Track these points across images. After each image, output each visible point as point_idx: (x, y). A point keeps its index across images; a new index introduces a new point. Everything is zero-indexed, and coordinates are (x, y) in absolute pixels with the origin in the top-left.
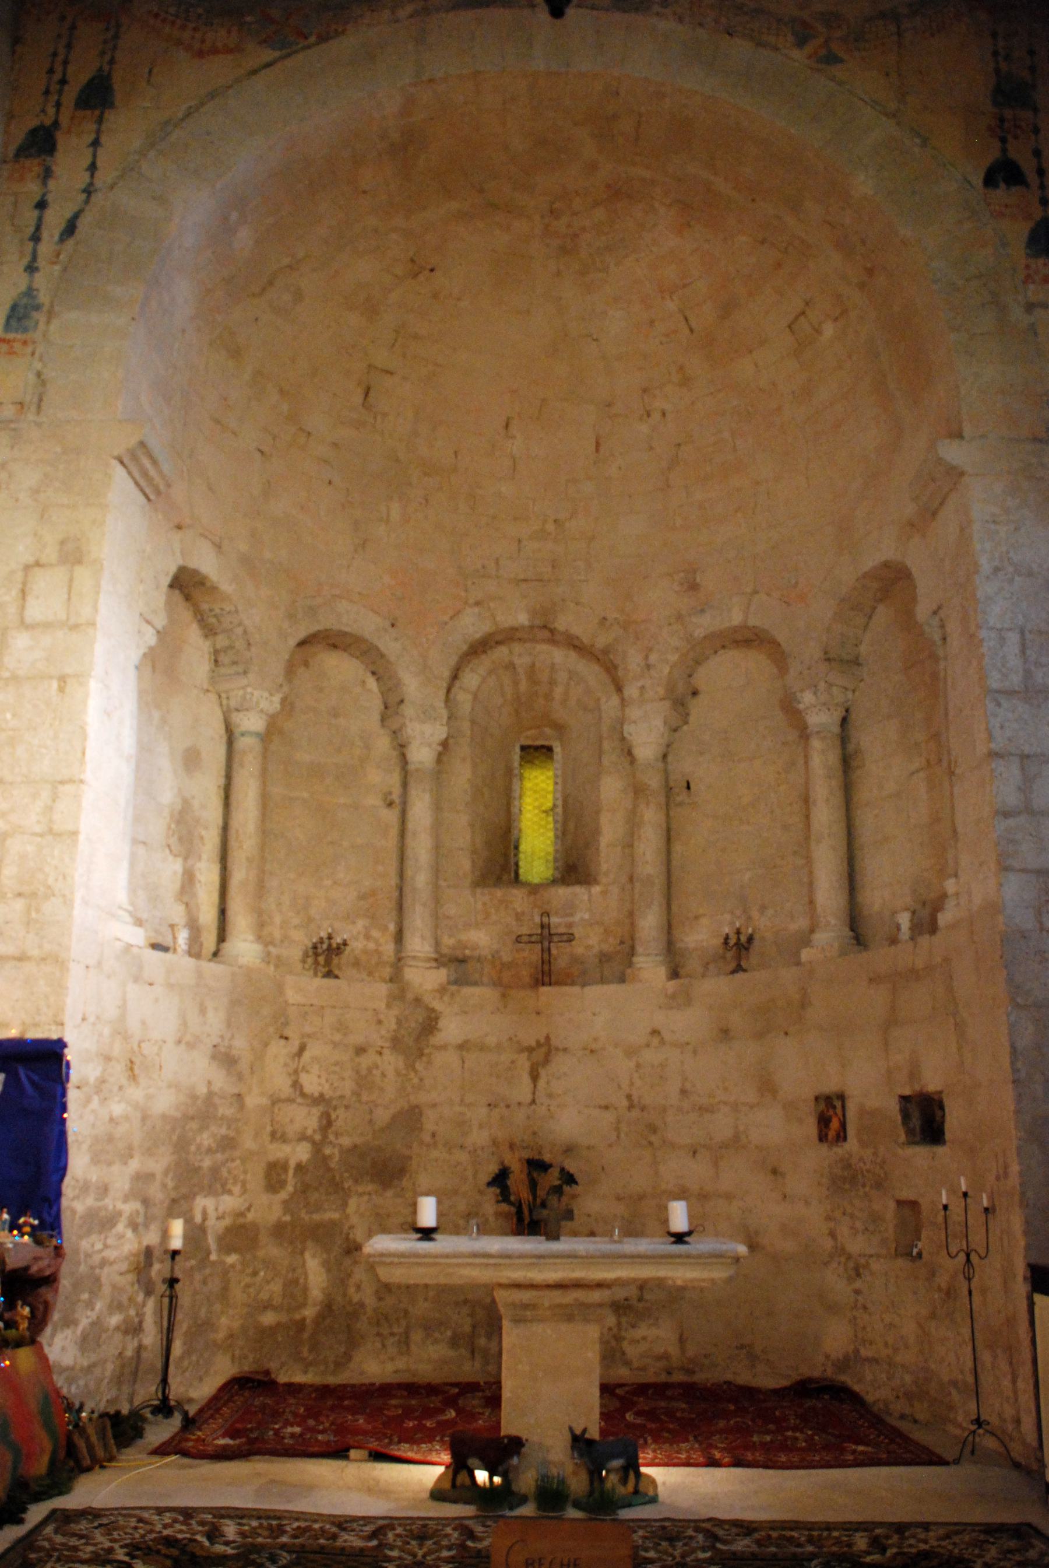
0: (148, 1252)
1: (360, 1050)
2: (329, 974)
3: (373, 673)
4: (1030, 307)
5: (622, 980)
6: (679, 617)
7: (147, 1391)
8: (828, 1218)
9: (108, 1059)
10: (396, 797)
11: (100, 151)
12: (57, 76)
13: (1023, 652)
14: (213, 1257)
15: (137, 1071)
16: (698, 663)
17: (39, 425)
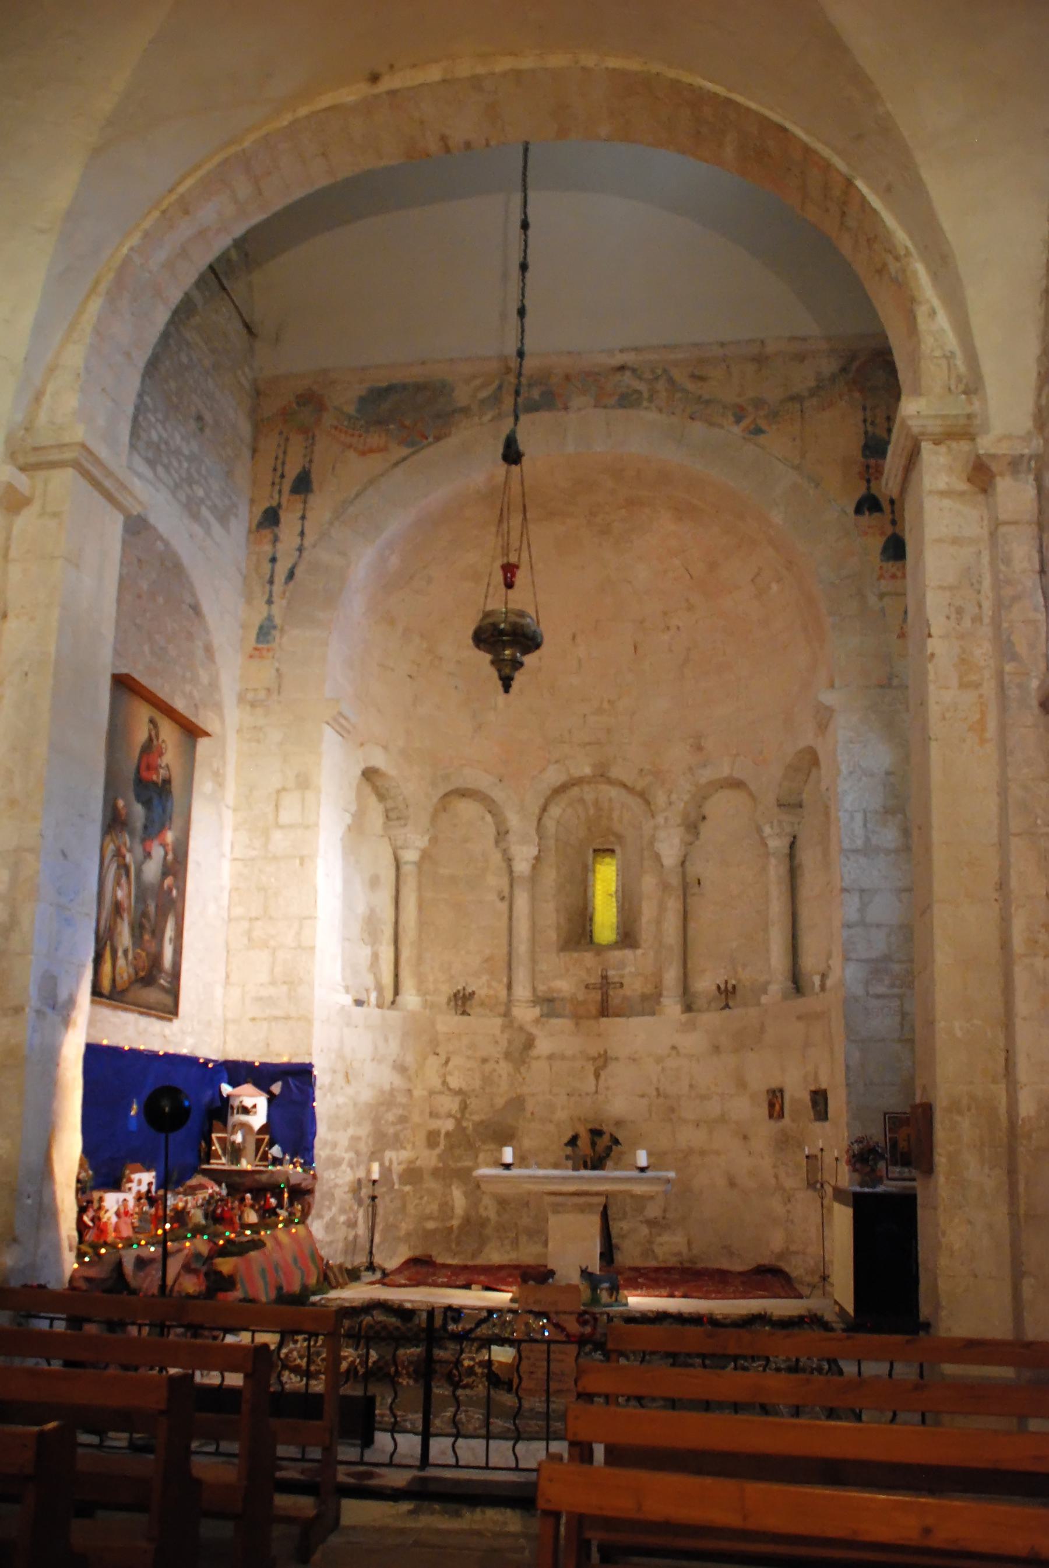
0: (359, 1181)
1: (484, 1061)
2: (464, 1013)
3: (490, 812)
4: (881, 596)
5: (653, 1013)
6: (690, 769)
7: (361, 1260)
8: (775, 1166)
9: (335, 1072)
10: (506, 893)
11: (306, 523)
12: (279, 473)
13: (865, 825)
14: (396, 1187)
15: (350, 1077)
16: (705, 798)
17: (280, 702)
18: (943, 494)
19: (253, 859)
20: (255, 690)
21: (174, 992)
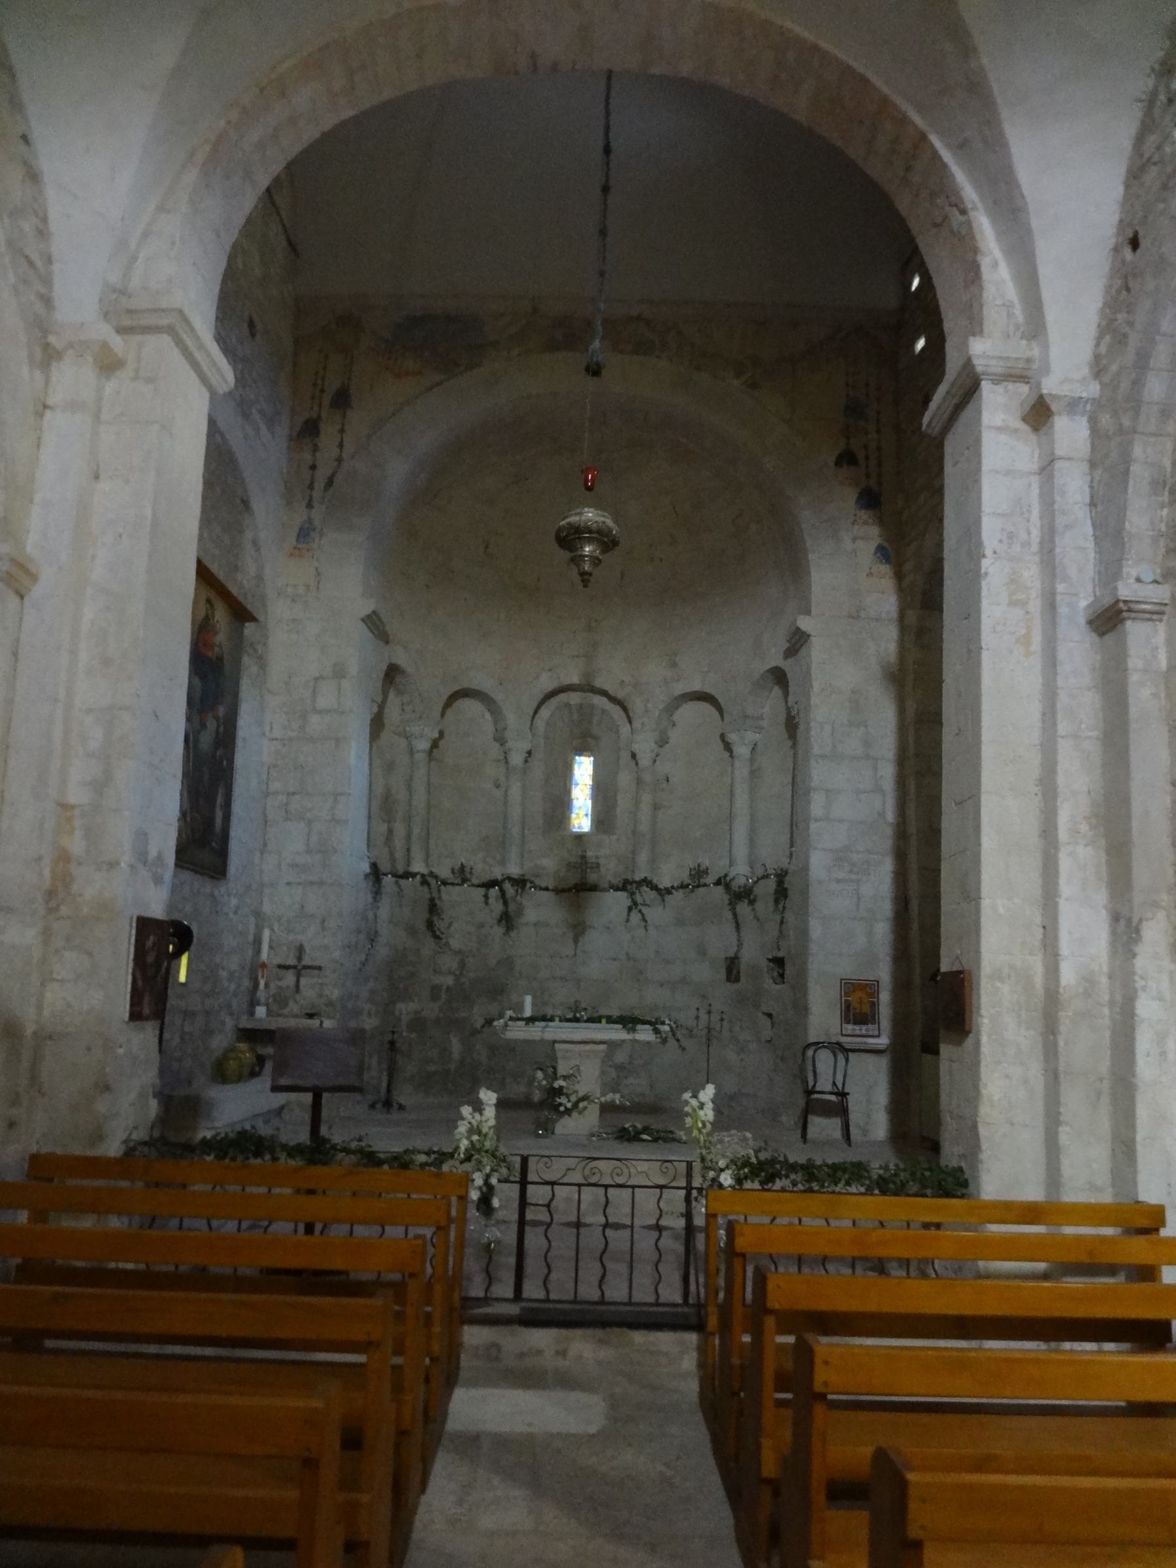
1: (481, 926)
4: (854, 539)
18: (999, 429)
19: (290, 739)
20: (295, 586)
21: (223, 854)
